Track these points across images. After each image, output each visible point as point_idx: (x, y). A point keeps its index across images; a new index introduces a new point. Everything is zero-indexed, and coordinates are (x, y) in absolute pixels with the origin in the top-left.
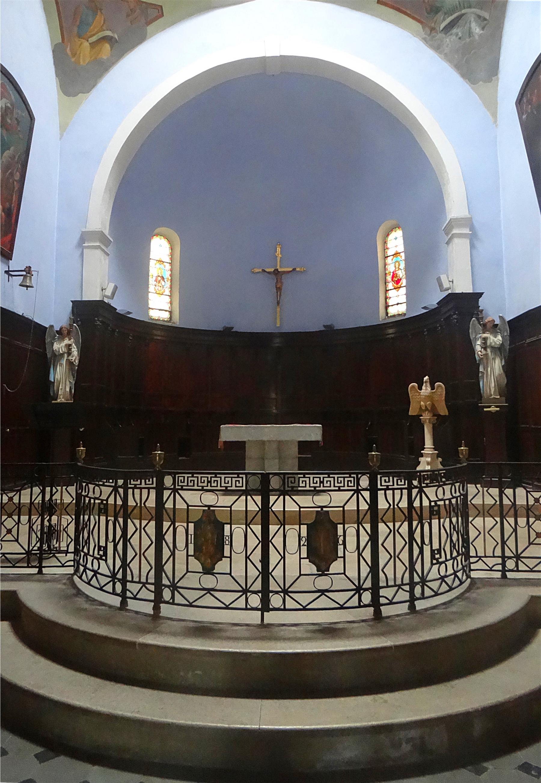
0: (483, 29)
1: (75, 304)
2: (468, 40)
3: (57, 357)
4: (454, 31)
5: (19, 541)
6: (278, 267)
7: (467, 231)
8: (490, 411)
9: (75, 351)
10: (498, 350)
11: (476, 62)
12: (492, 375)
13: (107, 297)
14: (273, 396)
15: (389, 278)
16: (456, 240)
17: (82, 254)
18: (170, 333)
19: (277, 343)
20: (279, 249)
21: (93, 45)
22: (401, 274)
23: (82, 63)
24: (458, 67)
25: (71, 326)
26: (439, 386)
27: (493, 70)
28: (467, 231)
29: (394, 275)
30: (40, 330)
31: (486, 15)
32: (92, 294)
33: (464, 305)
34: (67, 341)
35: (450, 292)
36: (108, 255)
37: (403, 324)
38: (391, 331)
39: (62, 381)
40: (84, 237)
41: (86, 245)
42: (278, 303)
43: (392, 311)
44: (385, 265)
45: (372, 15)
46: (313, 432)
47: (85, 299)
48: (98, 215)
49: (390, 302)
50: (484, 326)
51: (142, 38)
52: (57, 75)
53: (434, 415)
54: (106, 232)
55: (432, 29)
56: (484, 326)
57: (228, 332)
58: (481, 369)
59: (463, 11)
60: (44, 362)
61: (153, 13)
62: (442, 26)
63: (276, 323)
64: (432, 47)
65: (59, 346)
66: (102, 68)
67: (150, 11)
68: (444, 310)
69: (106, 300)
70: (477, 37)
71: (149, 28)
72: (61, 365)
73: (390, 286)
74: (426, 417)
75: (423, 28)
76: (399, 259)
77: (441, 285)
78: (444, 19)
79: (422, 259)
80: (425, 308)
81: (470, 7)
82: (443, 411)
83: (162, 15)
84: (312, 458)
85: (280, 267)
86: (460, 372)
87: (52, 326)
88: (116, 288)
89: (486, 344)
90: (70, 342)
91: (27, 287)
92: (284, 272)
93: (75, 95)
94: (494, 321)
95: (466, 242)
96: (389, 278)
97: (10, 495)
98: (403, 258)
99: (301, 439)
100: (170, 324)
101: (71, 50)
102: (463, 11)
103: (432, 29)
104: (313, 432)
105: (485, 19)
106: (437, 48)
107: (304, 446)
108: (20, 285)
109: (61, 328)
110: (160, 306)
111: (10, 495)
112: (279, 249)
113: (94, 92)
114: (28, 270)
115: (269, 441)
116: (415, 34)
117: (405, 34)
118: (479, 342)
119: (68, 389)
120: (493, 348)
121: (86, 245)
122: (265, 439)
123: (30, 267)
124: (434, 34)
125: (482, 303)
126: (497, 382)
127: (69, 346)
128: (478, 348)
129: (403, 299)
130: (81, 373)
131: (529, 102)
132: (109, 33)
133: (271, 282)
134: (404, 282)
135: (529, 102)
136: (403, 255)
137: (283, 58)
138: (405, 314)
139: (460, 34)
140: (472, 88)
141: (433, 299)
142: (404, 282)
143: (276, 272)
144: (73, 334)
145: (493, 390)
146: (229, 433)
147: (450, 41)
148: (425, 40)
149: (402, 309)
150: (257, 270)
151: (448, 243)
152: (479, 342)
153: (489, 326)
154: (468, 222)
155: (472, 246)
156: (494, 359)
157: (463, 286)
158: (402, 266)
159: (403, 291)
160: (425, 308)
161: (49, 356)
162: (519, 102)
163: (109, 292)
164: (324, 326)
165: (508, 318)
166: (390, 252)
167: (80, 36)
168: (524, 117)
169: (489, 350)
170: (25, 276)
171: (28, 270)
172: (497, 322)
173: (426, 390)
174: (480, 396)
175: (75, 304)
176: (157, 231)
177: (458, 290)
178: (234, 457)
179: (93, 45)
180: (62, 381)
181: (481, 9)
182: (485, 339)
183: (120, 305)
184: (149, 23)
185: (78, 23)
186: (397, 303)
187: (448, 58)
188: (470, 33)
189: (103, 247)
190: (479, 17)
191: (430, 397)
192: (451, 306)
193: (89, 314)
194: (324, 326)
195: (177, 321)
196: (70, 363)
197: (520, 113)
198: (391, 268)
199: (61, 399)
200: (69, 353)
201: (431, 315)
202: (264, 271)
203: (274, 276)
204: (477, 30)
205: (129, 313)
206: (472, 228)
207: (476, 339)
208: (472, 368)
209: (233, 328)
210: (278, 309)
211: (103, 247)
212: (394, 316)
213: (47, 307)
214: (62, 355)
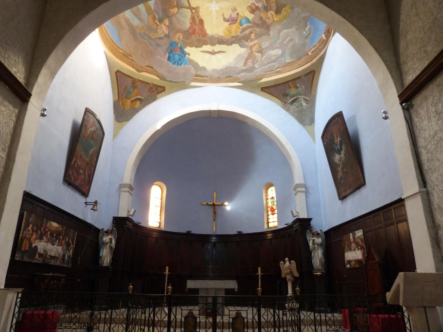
0: (307, 104)
1: (114, 217)
2: (301, 108)
3: (105, 244)
4: (295, 104)
5: (100, 329)
6: (215, 202)
7: (303, 189)
8: (317, 275)
9: (114, 242)
10: (321, 245)
11: (305, 117)
12: (318, 256)
13: (131, 215)
14: (211, 267)
15: (269, 209)
16: (299, 194)
17: (120, 194)
18: (162, 235)
19: (214, 239)
20: (215, 193)
21: (132, 102)
22: (275, 207)
23: (126, 108)
24: (297, 118)
25: (113, 229)
26: (293, 262)
27: (312, 121)
28: (303, 189)
29: (272, 208)
30: (97, 231)
31: (308, 99)
32: (123, 214)
33: (304, 224)
34: (110, 237)
35: (297, 217)
36: (132, 195)
37: (276, 232)
38: (269, 235)
39: (106, 256)
40: (121, 186)
41: (122, 190)
42: (214, 220)
43: (271, 225)
44: (267, 203)
45: (259, 95)
46: (232, 284)
47: (120, 216)
48: (128, 176)
49: (270, 221)
50: (313, 234)
51: (155, 99)
52: (114, 113)
53: (293, 277)
54: (132, 184)
55: (285, 103)
56: (313, 234)
57: (189, 234)
58: (313, 255)
59: (298, 96)
60: (97, 247)
61: (160, 89)
62: (289, 102)
63: (213, 229)
64: (285, 109)
65: (106, 239)
66: (135, 111)
67: (159, 88)
68: (295, 226)
69: (130, 217)
70: (304, 107)
71: (159, 96)
72: (106, 248)
73: (270, 213)
74: (288, 277)
75: (281, 102)
76: (273, 200)
77: (293, 214)
78: (290, 99)
79: (283, 201)
80: (286, 224)
81: (301, 95)
82: (297, 274)
83: (165, 90)
84: (232, 298)
85: (216, 202)
86: (303, 256)
87: (103, 229)
88: (135, 211)
89: (315, 242)
90: (111, 237)
91: (95, 210)
92: (217, 205)
93: (122, 122)
94: (317, 232)
95: (303, 195)
96: (269, 209)
97: (76, 314)
98: (276, 200)
99: (227, 287)
100: (159, 229)
101: (122, 103)
102: (298, 96)
103: (285, 103)
104: (232, 284)
105: (307, 100)
106: (288, 110)
107: (228, 291)
108: (91, 209)
109: (108, 230)
110: (154, 219)
111: (76, 314)
112: (215, 193)
113: (131, 121)
114: (96, 202)
115: (211, 289)
116: (279, 104)
117: (274, 103)
118: (311, 242)
119: (109, 261)
120: (317, 244)
121: (122, 190)
122: (209, 287)
123: (97, 201)
124: (286, 104)
125: (312, 223)
126: (320, 261)
127: (111, 239)
128: (311, 244)
129: (276, 219)
130: (116, 253)
131: (327, 138)
132: (140, 97)
133: (211, 209)
134: (276, 211)
135: (327, 138)
136: (275, 198)
137: (219, 111)
138: (277, 227)
139: (297, 105)
140: (304, 128)
141: (290, 220)
142: (276, 211)
143: (214, 205)
144: (114, 233)
145: (318, 265)
146: (191, 284)
147: (293, 107)
148: (282, 107)
149: (276, 224)
150: (204, 203)
151: (295, 195)
152: (311, 242)
153: (315, 234)
154: (305, 186)
155: (306, 196)
156: (318, 249)
157: (303, 215)
158: (275, 203)
159: (276, 216)
160: (286, 224)
161: (100, 243)
162: (323, 137)
163: (131, 213)
164: (237, 232)
165: (325, 230)
166: (269, 197)
167: (126, 98)
168: (325, 143)
169: (316, 246)
170: (94, 205)
171: (96, 202)
172: (319, 232)
173: (287, 263)
174: (313, 268)
175: (114, 217)
176: (155, 183)
177: (301, 217)
178: (192, 298)
179: (132, 102)
180: (106, 256)
181: (306, 96)
182: (314, 240)
183: (135, 219)
184: (158, 93)
185: (126, 92)
186: (274, 222)
187: (292, 114)
188: (301, 105)
189: (130, 191)
190: (305, 99)
191: (289, 268)
192: (298, 224)
193: (120, 223)
194: (237, 232)
195: (163, 227)
196: (111, 247)
197: (323, 141)
198: (270, 205)
199: (105, 265)
200: (111, 242)
201: (289, 227)
202: (207, 204)
203: (212, 207)
204: (304, 104)
205: (140, 223)
206: (306, 188)
207: (310, 240)
208: (309, 253)
209: (191, 232)
210: (214, 223)
211: (130, 191)
212: (271, 228)
213: (101, 220)
214: (107, 243)
